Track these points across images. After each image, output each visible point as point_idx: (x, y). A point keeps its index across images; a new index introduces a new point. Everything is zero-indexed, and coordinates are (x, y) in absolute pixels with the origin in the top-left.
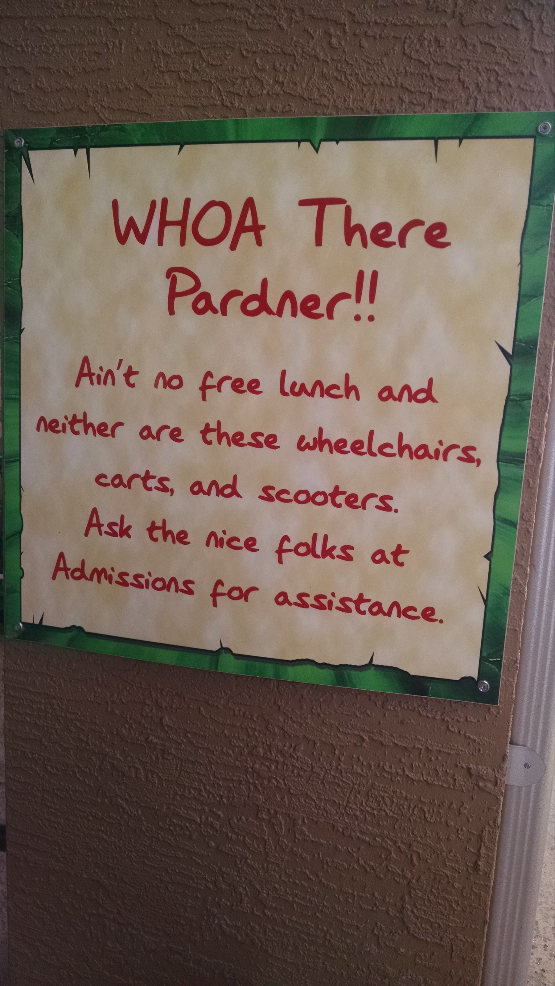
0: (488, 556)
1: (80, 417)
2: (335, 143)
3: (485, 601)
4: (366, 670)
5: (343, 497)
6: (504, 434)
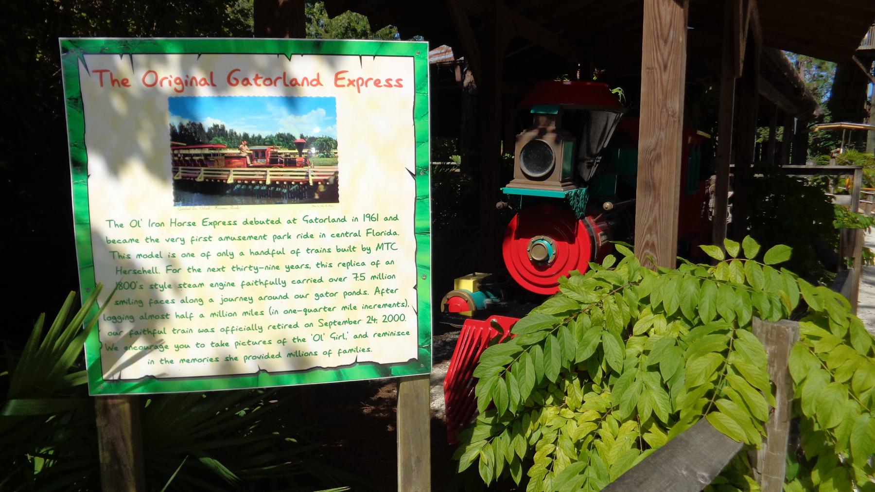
0: (415, 288)
2: (300, 56)
3: (417, 313)
4: (354, 366)
6: (416, 218)
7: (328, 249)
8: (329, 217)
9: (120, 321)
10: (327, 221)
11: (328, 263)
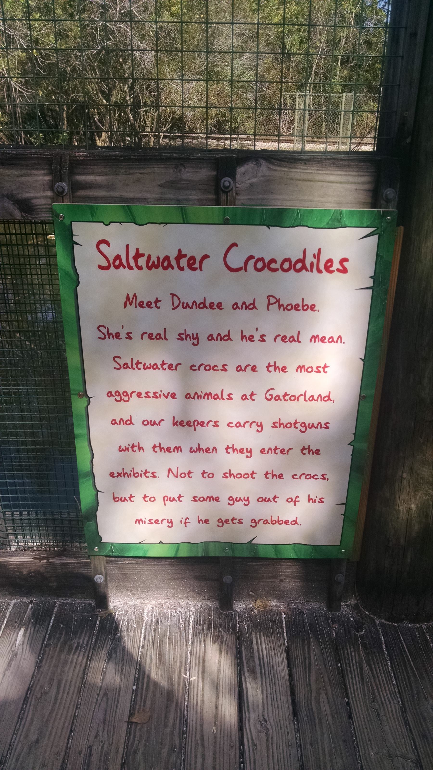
1: (136, 444)
2: (265, 227)
5: (148, 498)
7: (326, 424)
8: (306, 392)
9: (126, 398)
10: (302, 398)
11: (319, 498)
